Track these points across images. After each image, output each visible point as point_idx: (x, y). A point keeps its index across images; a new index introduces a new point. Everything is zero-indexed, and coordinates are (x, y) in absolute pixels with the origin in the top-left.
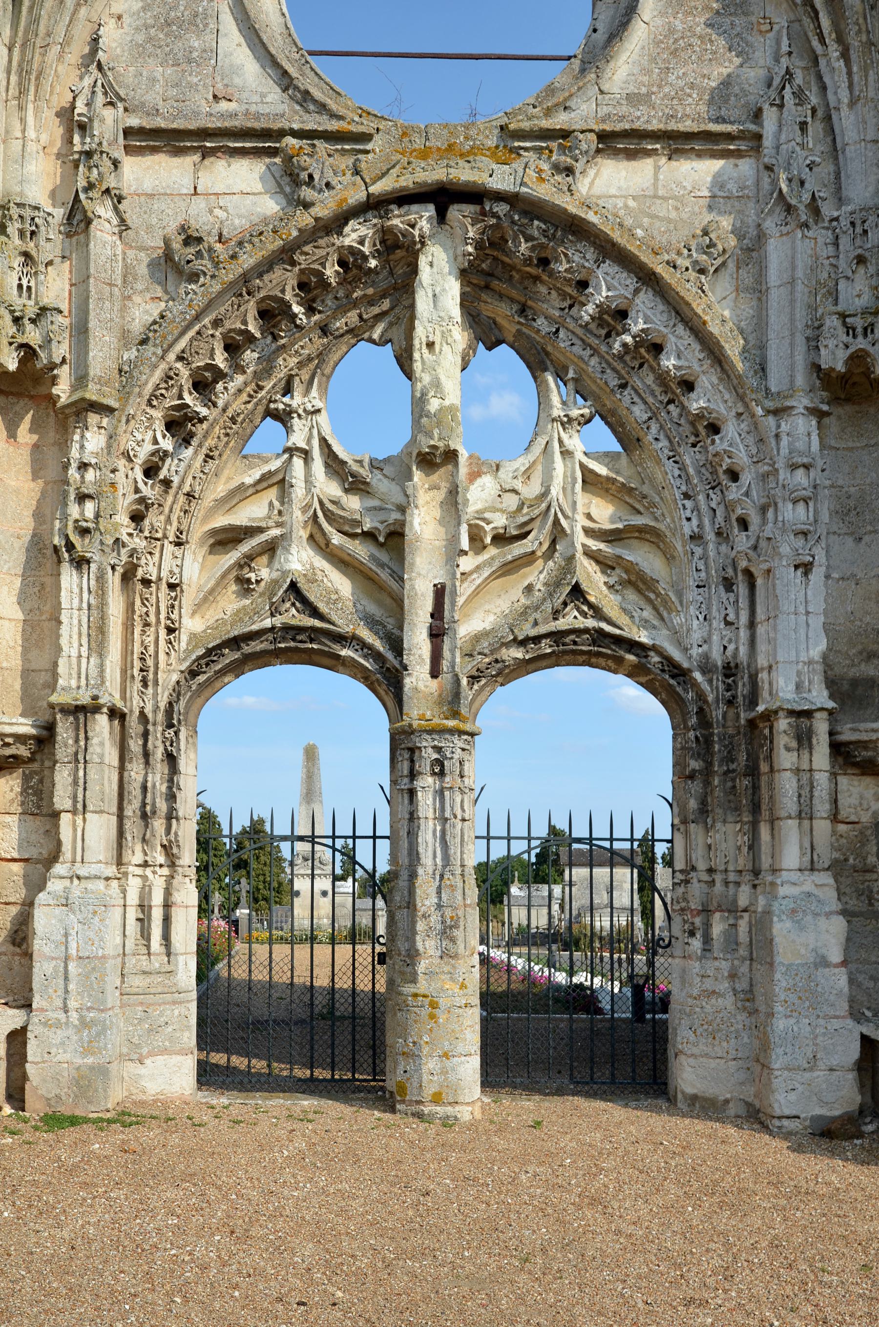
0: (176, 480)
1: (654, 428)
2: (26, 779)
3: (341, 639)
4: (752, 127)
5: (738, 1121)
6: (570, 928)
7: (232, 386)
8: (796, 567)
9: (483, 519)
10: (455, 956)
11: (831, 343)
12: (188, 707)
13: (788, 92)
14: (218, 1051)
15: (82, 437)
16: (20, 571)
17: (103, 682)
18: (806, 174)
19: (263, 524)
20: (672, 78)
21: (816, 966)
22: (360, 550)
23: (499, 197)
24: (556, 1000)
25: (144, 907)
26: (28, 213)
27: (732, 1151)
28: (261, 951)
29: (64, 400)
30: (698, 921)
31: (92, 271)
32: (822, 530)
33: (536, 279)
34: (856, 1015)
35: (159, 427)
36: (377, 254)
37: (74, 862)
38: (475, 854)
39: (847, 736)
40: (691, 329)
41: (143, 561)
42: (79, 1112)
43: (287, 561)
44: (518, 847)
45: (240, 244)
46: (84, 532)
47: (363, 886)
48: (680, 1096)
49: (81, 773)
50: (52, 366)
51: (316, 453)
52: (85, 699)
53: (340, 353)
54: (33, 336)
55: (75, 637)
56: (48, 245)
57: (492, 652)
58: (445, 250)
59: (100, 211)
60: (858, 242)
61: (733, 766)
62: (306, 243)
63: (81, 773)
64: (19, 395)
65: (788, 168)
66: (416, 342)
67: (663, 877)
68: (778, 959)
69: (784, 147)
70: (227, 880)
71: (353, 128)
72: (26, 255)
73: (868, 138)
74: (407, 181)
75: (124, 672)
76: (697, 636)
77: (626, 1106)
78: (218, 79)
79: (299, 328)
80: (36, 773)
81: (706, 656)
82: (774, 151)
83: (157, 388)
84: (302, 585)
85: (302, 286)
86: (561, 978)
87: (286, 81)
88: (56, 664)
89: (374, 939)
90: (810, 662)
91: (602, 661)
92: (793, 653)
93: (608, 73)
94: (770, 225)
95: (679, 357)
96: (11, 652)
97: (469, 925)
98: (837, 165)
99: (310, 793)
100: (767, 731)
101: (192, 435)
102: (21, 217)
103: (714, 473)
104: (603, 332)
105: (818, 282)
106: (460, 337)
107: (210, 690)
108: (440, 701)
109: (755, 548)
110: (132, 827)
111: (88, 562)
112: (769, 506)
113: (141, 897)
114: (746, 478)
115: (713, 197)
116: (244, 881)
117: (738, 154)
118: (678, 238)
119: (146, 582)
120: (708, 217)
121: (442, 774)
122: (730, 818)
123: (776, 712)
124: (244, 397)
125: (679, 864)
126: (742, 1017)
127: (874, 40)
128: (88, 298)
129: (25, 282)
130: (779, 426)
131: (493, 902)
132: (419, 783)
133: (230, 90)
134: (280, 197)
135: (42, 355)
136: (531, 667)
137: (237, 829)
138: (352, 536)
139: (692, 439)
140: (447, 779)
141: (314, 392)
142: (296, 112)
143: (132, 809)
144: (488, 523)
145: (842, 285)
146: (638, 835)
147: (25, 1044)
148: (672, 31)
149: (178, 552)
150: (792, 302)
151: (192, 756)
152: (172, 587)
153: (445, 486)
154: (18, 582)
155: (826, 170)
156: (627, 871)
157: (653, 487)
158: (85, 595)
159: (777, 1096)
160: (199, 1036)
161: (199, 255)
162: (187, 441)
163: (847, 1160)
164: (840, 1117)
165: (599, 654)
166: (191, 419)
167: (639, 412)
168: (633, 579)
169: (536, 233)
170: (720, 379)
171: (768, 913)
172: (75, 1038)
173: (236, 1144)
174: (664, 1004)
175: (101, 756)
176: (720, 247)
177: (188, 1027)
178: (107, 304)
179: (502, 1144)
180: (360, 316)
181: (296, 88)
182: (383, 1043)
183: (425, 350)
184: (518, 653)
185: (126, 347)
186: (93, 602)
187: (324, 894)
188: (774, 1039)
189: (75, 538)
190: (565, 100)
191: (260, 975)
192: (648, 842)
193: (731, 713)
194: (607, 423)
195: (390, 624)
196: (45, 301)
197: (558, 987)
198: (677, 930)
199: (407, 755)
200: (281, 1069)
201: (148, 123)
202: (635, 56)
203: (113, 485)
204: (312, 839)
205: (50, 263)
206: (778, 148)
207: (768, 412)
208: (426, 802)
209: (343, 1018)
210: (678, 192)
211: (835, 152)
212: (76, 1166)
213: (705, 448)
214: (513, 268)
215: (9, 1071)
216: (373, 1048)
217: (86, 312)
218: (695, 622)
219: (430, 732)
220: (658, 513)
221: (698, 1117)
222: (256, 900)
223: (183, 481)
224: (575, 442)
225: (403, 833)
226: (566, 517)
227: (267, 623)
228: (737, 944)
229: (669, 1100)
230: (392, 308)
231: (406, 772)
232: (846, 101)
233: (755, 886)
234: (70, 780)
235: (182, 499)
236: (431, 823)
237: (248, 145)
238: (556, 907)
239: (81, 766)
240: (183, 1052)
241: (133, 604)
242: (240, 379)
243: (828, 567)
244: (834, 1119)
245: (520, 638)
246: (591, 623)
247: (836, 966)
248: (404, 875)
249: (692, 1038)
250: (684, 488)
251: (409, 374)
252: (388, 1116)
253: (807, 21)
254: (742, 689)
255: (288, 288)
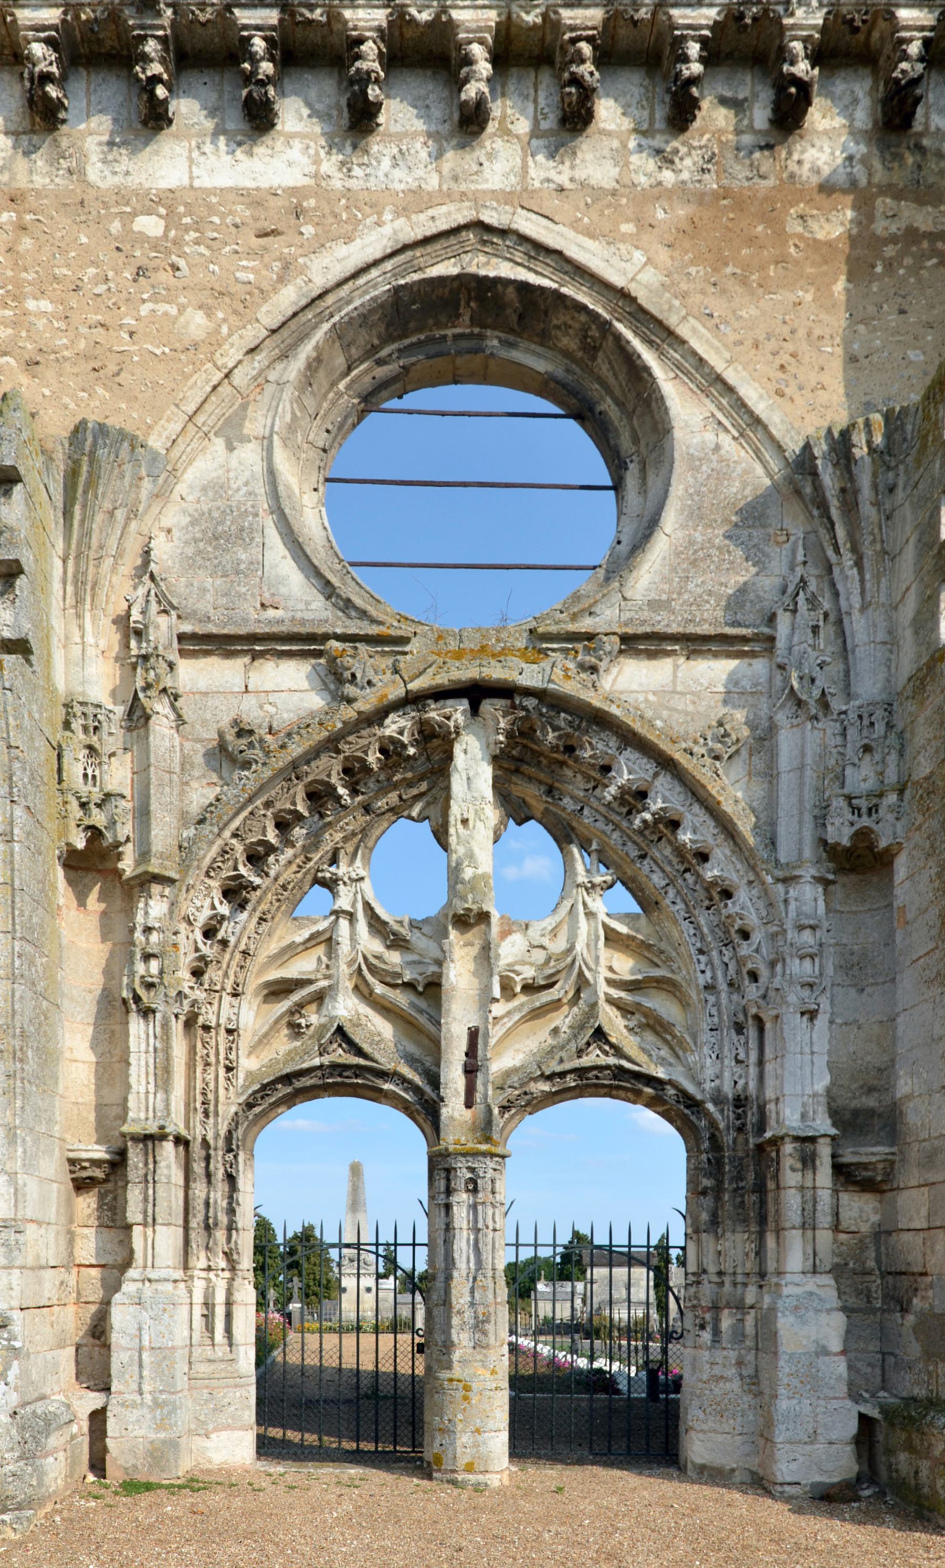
0: (232, 940)
1: (671, 893)
2: (101, 1197)
3: (383, 1075)
4: (766, 630)
5: (743, 1487)
6: (591, 1320)
7: (283, 858)
8: (803, 1014)
9: (514, 971)
10: (487, 1347)
11: (837, 821)
12: (245, 1134)
13: (801, 598)
14: (274, 1426)
15: (146, 904)
16: (91, 1020)
17: (169, 1114)
18: (817, 672)
19: (312, 977)
20: (691, 586)
21: (817, 1355)
22: (401, 999)
23: (528, 692)
24: (578, 1383)
25: (208, 1305)
26: (90, 710)
27: (737, 1513)
28: (312, 1340)
29: (129, 873)
30: (708, 1316)
31: (152, 760)
32: (827, 982)
33: (562, 764)
34: (854, 1396)
35: (217, 895)
36: (416, 743)
37: (145, 1267)
38: (505, 1257)
39: (848, 1157)
40: (707, 808)
41: (203, 1010)
42: (153, 1479)
43: (334, 1008)
44: (545, 1253)
45: (289, 735)
46: (150, 986)
47: (403, 1283)
48: (689, 1466)
49: (151, 1192)
50: (118, 844)
51: (360, 915)
52: (153, 1128)
53: (381, 829)
54: (98, 818)
55: (143, 1076)
56: (111, 739)
57: (522, 1086)
58: (479, 739)
59: (158, 707)
60: (865, 733)
61: (742, 1184)
62: (350, 734)
63: (151, 1192)
64: (87, 870)
65: (799, 666)
66: (452, 820)
67: (676, 1276)
68: (782, 1349)
69: (796, 648)
70: (281, 1278)
71: (392, 632)
72: (90, 748)
73: (878, 639)
74: (441, 680)
75: (187, 1105)
76: (709, 1072)
77: (640, 1474)
78: (265, 588)
79: (344, 807)
80: (110, 1191)
81: (718, 1090)
82: (786, 653)
83: (214, 861)
84: (348, 1029)
85: (346, 771)
86: (582, 1363)
87: (328, 590)
88: (126, 1100)
89: (414, 1332)
90: (815, 1095)
91: (622, 1093)
92: (799, 1088)
93: (631, 581)
94: (781, 717)
95: (695, 832)
96: (85, 1090)
97: (499, 1320)
98: (847, 664)
99: (355, 1204)
100: (774, 1155)
101: (246, 901)
102: (84, 714)
103: (727, 932)
104: (625, 810)
105: (826, 768)
106: (492, 814)
107: (265, 1120)
108: (474, 1128)
109: (764, 997)
110: (197, 1237)
111: (154, 1012)
112: (777, 961)
113: (206, 1296)
114: (756, 937)
115: (728, 692)
116: (296, 1279)
117: (752, 654)
118: (694, 729)
119: (207, 1028)
120: (724, 710)
121: (475, 1191)
122: (739, 1229)
123: (782, 1138)
124: (294, 867)
125: (691, 1267)
126: (748, 1398)
127: (888, 549)
128: (148, 784)
129: (90, 772)
130: (787, 893)
131: (521, 1296)
132: (454, 1199)
133: (276, 599)
134: (326, 694)
135: (108, 835)
136: (556, 1098)
137: (290, 1235)
138: (394, 986)
139: (707, 903)
140: (480, 1195)
141: (358, 862)
142: (339, 618)
143: (196, 1222)
144: (518, 974)
145: (849, 771)
146: (654, 1242)
147: (104, 1422)
148: (692, 542)
149: (235, 1001)
150: (801, 785)
151: (250, 1175)
152: (230, 1032)
153: (478, 944)
154: (90, 1030)
155: (836, 669)
156: (644, 1270)
157: (671, 943)
158: (152, 1040)
159: (779, 1465)
160: (257, 1414)
161: (251, 745)
162: (242, 906)
163: (844, 1520)
164: (839, 1483)
165: (619, 1088)
166: (245, 888)
167: (658, 879)
168: (651, 1022)
169: (562, 724)
170: (733, 852)
171: (773, 1310)
172: (149, 1416)
173: (291, 1507)
174: (677, 1385)
175: (168, 1177)
176: (734, 737)
177: (248, 1407)
178: (167, 789)
179: (527, 1507)
180: (400, 797)
181: (339, 596)
182: (422, 1421)
183: (460, 826)
184: (545, 1087)
185: (185, 826)
186: (158, 1045)
187: (369, 1290)
188: (778, 1417)
189: (141, 992)
190: (591, 606)
191: (312, 1360)
192: (663, 1248)
193: (741, 1139)
194: (628, 888)
195: (428, 1061)
196: (109, 788)
197: (580, 1371)
198: (688, 1324)
199: (443, 1175)
200: (330, 1442)
201: (200, 629)
202: (656, 566)
203: (175, 945)
204: (358, 1246)
205: (113, 755)
206: (790, 649)
207: (778, 880)
208: (461, 1215)
209: (385, 1397)
210: (696, 688)
211: (845, 652)
212: (151, 1526)
213: (719, 911)
214: (541, 754)
215: (92, 1444)
216: (413, 1424)
217: (148, 797)
218: (709, 1061)
219: (464, 1155)
220: (675, 966)
221: (706, 1484)
222: (307, 1296)
223: (239, 941)
224: (598, 904)
225: (440, 1241)
226: (590, 969)
227: (317, 1062)
228: (744, 1336)
229: (679, 1469)
230: (429, 790)
231: (442, 1189)
232: (857, 606)
233: (761, 1287)
234: (141, 1197)
235: (238, 956)
236: (465, 1233)
237: (294, 648)
238: (578, 1302)
239: (151, 1185)
240: (244, 1428)
241: (195, 1047)
242: (289, 852)
243: (832, 1014)
244: (833, 1485)
245: (547, 1073)
246: (612, 1060)
247: (836, 1354)
248: (441, 1277)
249: (702, 1416)
250: (699, 945)
251: (445, 846)
252: (425, 1483)
253: (823, 532)
254: (751, 1118)
255: (334, 773)
